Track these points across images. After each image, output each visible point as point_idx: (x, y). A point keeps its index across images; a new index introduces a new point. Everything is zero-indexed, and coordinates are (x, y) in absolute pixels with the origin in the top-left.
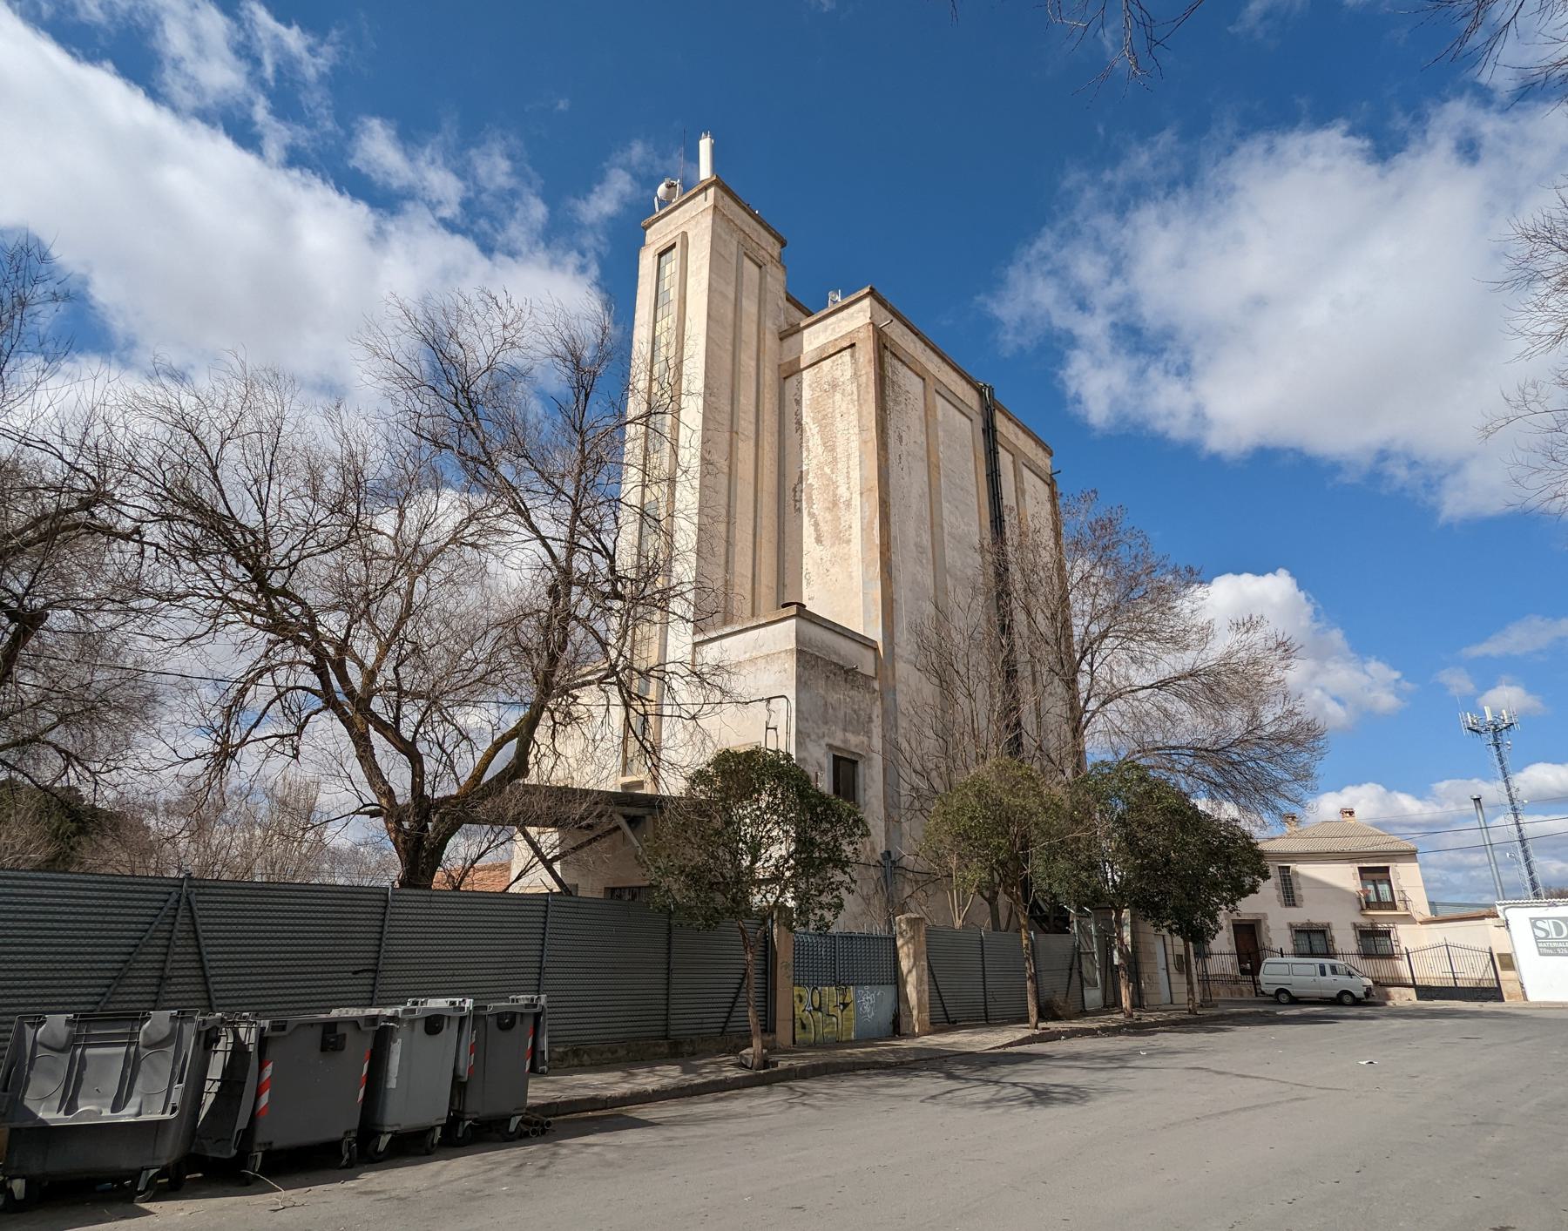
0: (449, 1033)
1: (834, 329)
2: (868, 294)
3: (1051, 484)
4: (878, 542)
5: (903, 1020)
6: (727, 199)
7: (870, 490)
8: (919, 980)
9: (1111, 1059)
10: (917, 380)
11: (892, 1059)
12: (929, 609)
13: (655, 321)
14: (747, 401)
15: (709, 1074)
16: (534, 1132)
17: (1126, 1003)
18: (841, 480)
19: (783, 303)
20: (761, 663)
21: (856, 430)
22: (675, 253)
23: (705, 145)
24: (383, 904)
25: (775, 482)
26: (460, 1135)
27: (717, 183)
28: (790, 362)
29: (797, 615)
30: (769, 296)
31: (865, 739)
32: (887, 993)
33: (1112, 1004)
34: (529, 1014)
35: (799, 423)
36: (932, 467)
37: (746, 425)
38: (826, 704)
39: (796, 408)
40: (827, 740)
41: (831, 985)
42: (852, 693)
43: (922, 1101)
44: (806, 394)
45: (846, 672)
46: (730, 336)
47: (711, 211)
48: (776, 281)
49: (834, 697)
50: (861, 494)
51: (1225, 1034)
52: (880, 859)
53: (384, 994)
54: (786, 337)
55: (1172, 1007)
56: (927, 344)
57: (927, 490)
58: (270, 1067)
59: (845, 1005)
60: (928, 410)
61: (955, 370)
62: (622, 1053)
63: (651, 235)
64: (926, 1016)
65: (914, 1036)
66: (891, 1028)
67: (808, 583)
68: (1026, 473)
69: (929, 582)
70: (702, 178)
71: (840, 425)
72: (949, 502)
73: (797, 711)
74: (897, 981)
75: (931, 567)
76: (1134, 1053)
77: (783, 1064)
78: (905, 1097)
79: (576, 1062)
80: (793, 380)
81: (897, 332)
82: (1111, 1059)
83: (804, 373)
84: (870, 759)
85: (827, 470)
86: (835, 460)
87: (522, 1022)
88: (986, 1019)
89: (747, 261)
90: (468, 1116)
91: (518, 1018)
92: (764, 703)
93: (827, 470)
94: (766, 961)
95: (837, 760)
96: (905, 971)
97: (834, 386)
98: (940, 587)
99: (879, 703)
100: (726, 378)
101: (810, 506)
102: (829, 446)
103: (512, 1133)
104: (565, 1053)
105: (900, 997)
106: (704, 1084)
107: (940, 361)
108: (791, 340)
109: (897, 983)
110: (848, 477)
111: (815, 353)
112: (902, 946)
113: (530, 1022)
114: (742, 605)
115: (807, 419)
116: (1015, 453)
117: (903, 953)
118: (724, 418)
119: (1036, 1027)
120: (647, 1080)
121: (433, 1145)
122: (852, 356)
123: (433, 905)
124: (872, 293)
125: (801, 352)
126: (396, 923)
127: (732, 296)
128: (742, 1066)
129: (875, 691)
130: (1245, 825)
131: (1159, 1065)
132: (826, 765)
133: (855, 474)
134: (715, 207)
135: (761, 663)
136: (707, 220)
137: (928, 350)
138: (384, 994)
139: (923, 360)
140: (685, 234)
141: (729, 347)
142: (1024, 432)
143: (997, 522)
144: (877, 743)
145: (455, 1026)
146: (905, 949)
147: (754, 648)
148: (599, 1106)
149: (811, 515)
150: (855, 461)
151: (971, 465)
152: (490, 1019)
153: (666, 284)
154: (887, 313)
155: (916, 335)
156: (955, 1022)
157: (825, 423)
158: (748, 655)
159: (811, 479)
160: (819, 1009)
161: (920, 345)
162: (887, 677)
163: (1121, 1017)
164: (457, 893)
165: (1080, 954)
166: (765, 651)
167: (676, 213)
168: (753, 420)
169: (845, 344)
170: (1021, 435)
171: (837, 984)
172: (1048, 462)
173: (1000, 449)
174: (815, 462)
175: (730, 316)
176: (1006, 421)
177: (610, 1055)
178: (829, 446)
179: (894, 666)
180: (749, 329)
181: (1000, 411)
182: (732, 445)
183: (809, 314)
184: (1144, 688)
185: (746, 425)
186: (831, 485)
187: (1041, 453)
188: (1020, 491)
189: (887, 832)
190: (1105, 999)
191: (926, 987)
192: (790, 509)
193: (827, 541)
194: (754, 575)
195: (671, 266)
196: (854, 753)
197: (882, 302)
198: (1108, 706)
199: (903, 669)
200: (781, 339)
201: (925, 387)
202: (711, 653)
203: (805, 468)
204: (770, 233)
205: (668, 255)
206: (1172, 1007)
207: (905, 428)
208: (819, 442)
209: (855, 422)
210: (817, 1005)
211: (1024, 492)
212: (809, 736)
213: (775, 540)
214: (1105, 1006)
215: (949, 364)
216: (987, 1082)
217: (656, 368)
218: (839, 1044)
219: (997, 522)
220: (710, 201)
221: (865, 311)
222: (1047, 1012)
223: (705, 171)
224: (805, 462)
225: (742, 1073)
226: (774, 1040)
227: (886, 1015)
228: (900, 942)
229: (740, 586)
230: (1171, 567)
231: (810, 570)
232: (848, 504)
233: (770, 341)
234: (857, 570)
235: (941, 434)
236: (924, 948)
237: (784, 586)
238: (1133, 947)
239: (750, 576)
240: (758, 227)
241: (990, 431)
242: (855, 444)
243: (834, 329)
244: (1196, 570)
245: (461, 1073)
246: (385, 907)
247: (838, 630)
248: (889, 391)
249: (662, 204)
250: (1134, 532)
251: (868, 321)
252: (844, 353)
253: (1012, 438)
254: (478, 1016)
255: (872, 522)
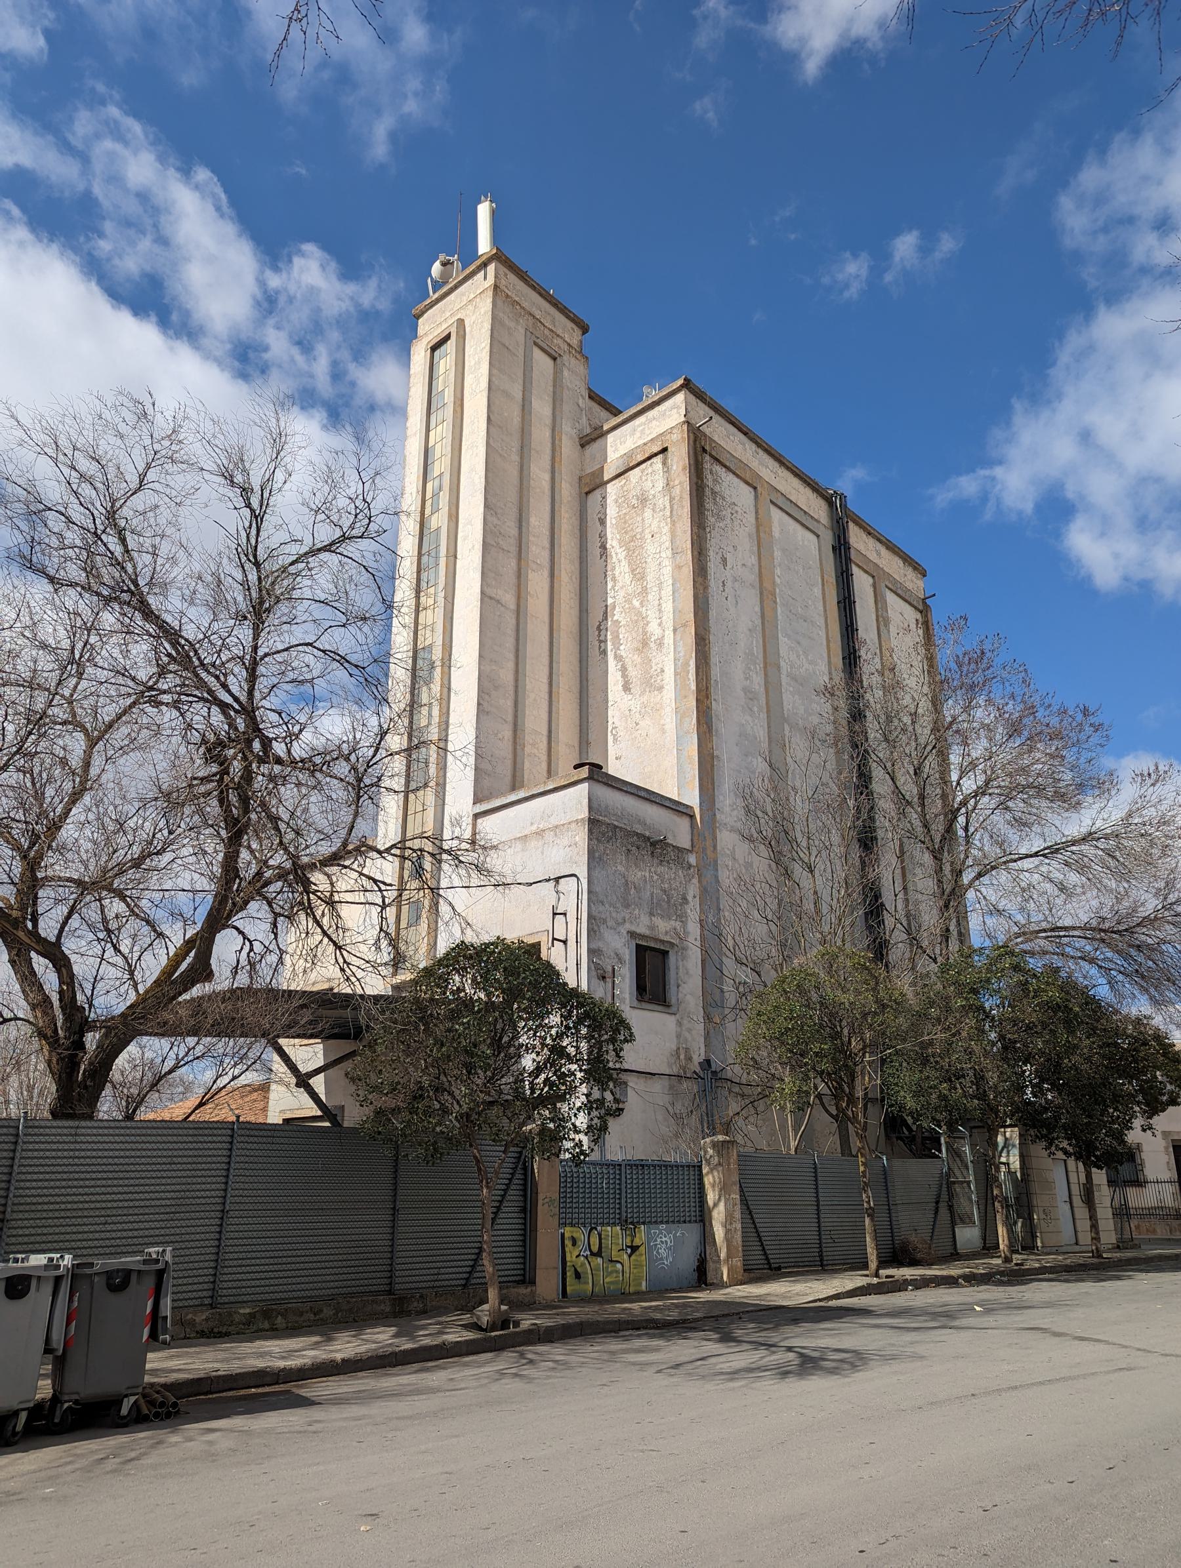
0: (40, 1297)
1: (642, 432)
2: (682, 386)
3: (924, 609)
4: (694, 687)
5: (711, 1266)
6: (512, 277)
7: (685, 625)
8: (729, 1217)
9: (935, 1315)
10: (747, 491)
11: (674, 1315)
12: (761, 766)
13: (428, 430)
14: (538, 521)
15: (426, 1337)
16: (157, 1415)
17: (1003, 1244)
18: (652, 615)
19: (585, 402)
20: (549, 836)
21: (669, 553)
22: (451, 346)
23: (484, 211)
24: (12, 1139)
25: (576, 620)
26: (56, 1421)
27: (498, 257)
28: (593, 474)
29: (590, 778)
30: (566, 394)
31: (678, 925)
32: (689, 1234)
33: (989, 1247)
34: (47, 1278)
35: (604, 547)
36: (766, 595)
37: (538, 550)
38: (627, 884)
39: (600, 528)
40: (628, 926)
41: (614, 1224)
42: (660, 869)
43: (659, 1372)
44: (612, 511)
45: (653, 844)
46: (515, 444)
47: (490, 293)
48: (575, 376)
49: (636, 875)
50: (675, 630)
51: (1119, 1283)
52: (698, 1070)
53: (13, 1240)
54: (588, 443)
55: (1077, 1248)
56: (759, 445)
57: (758, 622)
58: (148, 1310)
59: (634, 1249)
60: (761, 526)
61: (796, 475)
62: (328, 1312)
63: (424, 325)
64: (738, 1262)
65: (723, 1286)
66: (696, 1275)
67: (615, 740)
68: (891, 598)
69: (762, 733)
70: (480, 253)
71: (651, 548)
72: (789, 637)
73: (589, 892)
74: (702, 1217)
75: (764, 716)
76: (967, 1309)
77: (527, 1322)
78: (643, 1366)
79: (266, 1325)
80: (597, 494)
81: (720, 433)
82: (935, 1315)
83: (609, 486)
84: (685, 949)
85: (636, 603)
86: (645, 591)
87: (38, 1289)
88: (822, 1266)
89: (537, 352)
90: (66, 1398)
91: (134, 1277)
92: (552, 883)
93: (636, 603)
94: (525, 1196)
95: (641, 951)
96: (711, 1203)
97: (643, 500)
98: (777, 742)
99: (695, 881)
100: (512, 495)
101: (617, 644)
102: (639, 574)
103: (124, 1417)
104: (252, 1315)
105: (706, 1236)
106: (412, 1350)
107: (776, 465)
108: (595, 447)
109: (702, 1221)
110: (660, 611)
111: (621, 461)
112: (708, 1173)
113: (150, 1282)
114: (535, 765)
115: (612, 542)
116: (875, 573)
117: (708, 1180)
118: (510, 544)
119: (877, 1276)
120: (345, 1347)
121: (14, 1434)
122: (664, 463)
123: (79, 1139)
124: (687, 385)
125: (605, 460)
126: (30, 1154)
127: (518, 395)
128: (476, 1327)
129: (690, 866)
130: (1158, 1021)
131: (993, 1324)
132: (627, 957)
133: (668, 606)
134: (496, 287)
135: (549, 836)
136: (486, 304)
137: (761, 452)
138: (13, 1240)
139: (754, 464)
140: (461, 322)
141: (516, 458)
142: (888, 548)
143: (851, 659)
144: (694, 929)
145: (48, 1289)
146: (710, 1177)
147: (542, 818)
148: (268, 1380)
149: (618, 658)
150: (668, 591)
151: (817, 591)
152: (96, 1279)
153: (439, 384)
154: (707, 408)
155: (745, 434)
156: (779, 1268)
157: (633, 546)
158: (534, 828)
159: (617, 615)
160: (599, 1254)
161: (751, 447)
162: (704, 850)
163: (999, 1261)
164: (129, 1124)
165: (950, 1185)
166: (554, 821)
167: (452, 296)
168: (548, 545)
169: (656, 449)
170: (884, 551)
171: (624, 1223)
172: (920, 583)
173: (855, 569)
174: (622, 593)
175: (517, 421)
176: (864, 536)
177: (312, 1317)
178: (639, 574)
179: (715, 838)
180: (541, 434)
181: (855, 522)
182: (520, 574)
183: (616, 412)
184: (1027, 856)
185: (538, 550)
186: (640, 620)
187: (910, 574)
188: (882, 620)
189: (707, 1036)
190: (984, 1239)
191: (739, 1226)
192: (594, 652)
193: (636, 689)
194: (550, 731)
195: (446, 362)
196: (663, 942)
197: (699, 395)
198: (985, 880)
199: (727, 840)
200: (583, 446)
201: (756, 497)
202: (488, 825)
203: (610, 601)
204: (568, 317)
205: (443, 348)
206: (1077, 1248)
207: (731, 549)
208: (627, 569)
209: (668, 544)
210: (595, 1249)
211: (887, 622)
212: (605, 921)
213: (576, 689)
214: (984, 1248)
215: (788, 468)
216: (758, 1345)
217: (429, 486)
218: (625, 1296)
219: (851, 659)
220: (491, 279)
221: (678, 408)
222: (896, 1255)
223: (484, 245)
224: (611, 593)
225: (470, 1335)
226: (533, 1293)
227: (688, 1261)
228: (705, 1170)
229: (533, 745)
230: (1055, 708)
231: (617, 724)
232: (660, 643)
233: (568, 447)
234: (669, 721)
235: (777, 554)
236: (736, 1178)
237: (588, 743)
238: (1022, 1174)
239: (545, 732)
240: (553, 311)
241: (842, 549)
242: (667, 570)
243: (642, 432)
244: (1091, 710)
245: (54, 1345)
246: (16, 1143)
247: (643, 794)
248: (709, 505)
249: (437, 286)
250: (1016, 666)
251: (683, 419)
252: (654, 460)
253: (872, 556)
254: (77, 1275)
255: (687, 664)
